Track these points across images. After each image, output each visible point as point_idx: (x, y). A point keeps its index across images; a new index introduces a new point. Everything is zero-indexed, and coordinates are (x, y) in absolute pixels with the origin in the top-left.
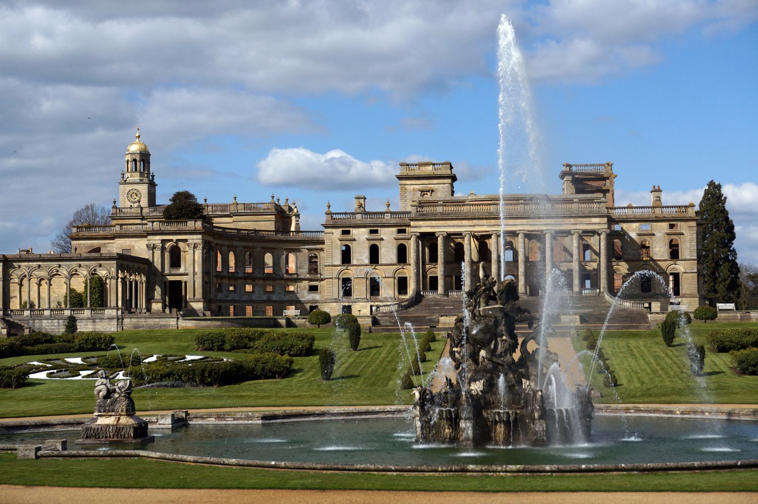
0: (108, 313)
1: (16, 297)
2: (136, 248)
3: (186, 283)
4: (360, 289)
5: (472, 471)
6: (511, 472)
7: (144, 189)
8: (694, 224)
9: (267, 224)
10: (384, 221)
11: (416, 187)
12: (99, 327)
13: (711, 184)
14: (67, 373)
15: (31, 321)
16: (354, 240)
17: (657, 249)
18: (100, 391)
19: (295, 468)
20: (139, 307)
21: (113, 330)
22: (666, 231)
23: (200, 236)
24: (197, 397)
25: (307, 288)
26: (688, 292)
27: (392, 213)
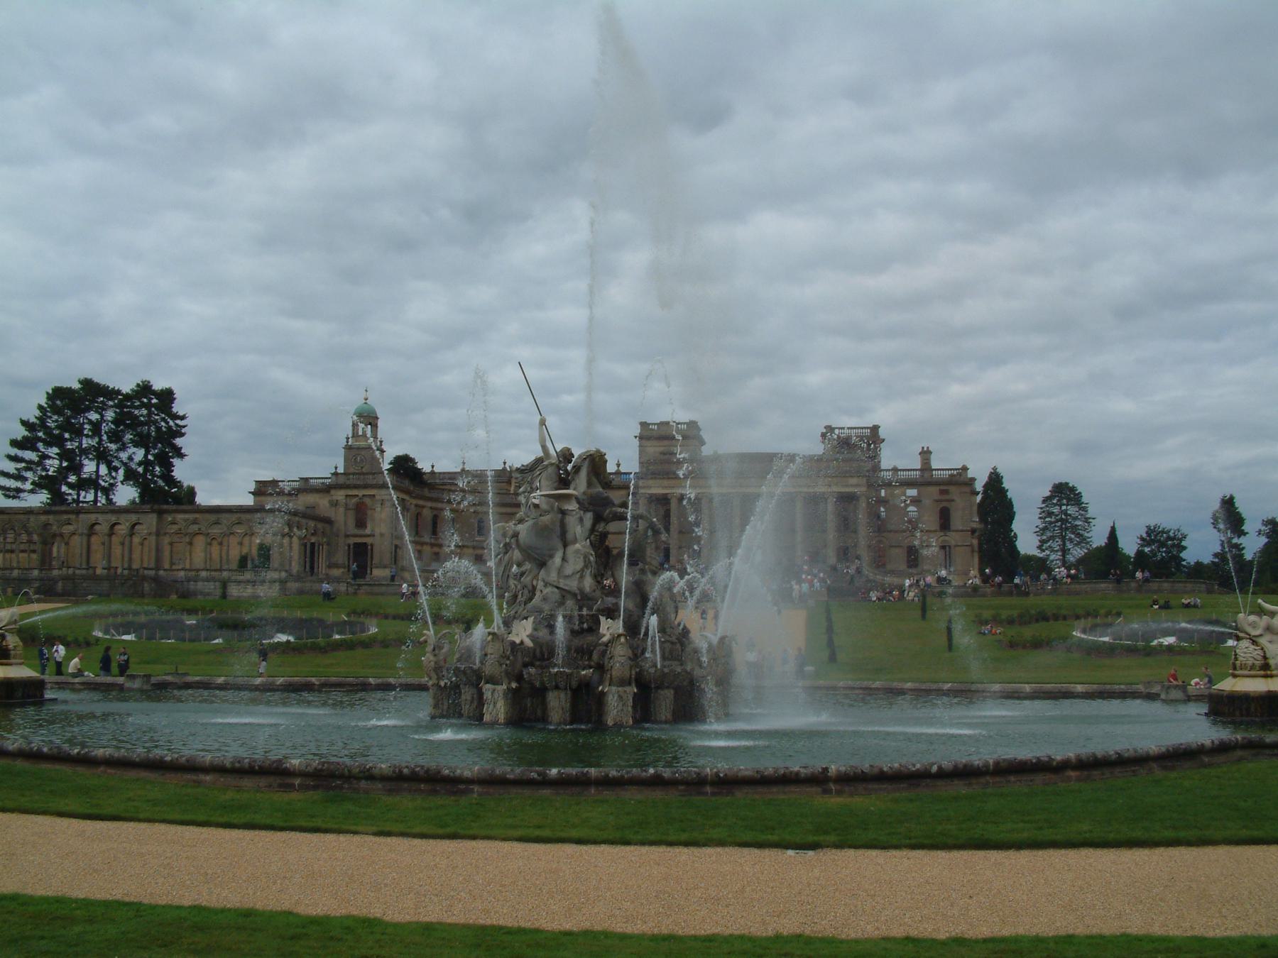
3: (372, 545)
15: (185, 583)
22: (936, 498)
24: (682, 650)
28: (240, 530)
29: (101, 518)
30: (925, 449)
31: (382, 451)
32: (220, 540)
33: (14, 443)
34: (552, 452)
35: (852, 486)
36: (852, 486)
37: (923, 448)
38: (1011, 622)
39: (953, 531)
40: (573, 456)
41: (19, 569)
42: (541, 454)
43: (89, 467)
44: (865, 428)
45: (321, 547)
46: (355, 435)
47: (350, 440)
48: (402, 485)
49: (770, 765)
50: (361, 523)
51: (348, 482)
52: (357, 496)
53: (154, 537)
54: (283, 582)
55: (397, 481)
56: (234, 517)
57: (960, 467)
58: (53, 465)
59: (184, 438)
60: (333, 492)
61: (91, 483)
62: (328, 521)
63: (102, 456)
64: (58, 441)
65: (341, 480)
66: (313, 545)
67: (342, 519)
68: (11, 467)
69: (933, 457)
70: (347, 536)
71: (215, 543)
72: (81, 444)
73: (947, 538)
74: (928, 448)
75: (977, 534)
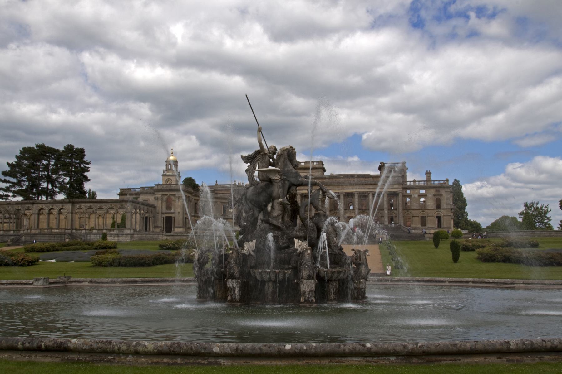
0: (127, 231)
1: (87, 225)
2: (150, 200)
3: (174, 217)
12: (121, 239)
13: (455, 180)
15: (86, 236)
17: (429, 203)
20: (148, 229)
21: (128, 240)
22: (433, 194)
28: (112, 211)
29: (44, 206)
30: (428, 172)
31: (180, 177)
32: (103, 216)
33: (4, 173)
34: (265, 147)
35: (395, 188)
36: (395, 188)
37: (427, 171)
39: (443, 209)
40: (276, 150)
41: (3, 230)
42: (259, 148)
43: (44, 185)
45: (150, 219)
46: (168, 170)
47: (165, 172)
48: (188, 190)
50: (169, 208)
51: (163, 189)
52: (167, 195)
53: (70, 215)
54: (132, 235)
55: (186, 188)
56: (109, 205)
57: (445, 179)
58: (25, 185)
59: (89, 172)
60: (156, 193)
61: (45, 192)
62: (154, 207)
63: (49, 180)
64: (27, 173)
65: (160, 188)
66: (146, 218)
67: (161, 206)
68: (4, 185)
69: (432, 175)
70: (162, 213)
71: (101, 217)
72: (39, 174)
73: (439, 212)
74: (429, 171)
75: (453, 211)
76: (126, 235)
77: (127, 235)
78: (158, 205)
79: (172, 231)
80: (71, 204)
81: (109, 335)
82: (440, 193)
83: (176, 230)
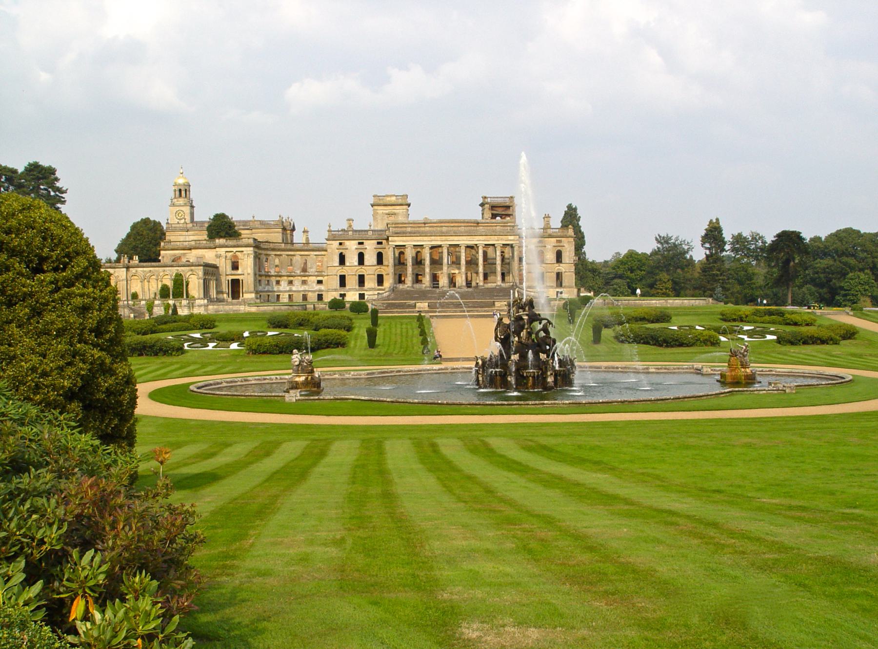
2: (206, 257)
3: (242, 280)
4: (352, 282)
5: (547, 404)
6: (566, 404)
7: (187, 210)
8: (572, 240)
9: (276, 236)
10: (367, 236)
11: (384, 211)
14: (199, 345)
16: (347, 249)
17: (548, 256)
18: (296, 361)
19: (469, 405)
23: (252, 249)
25: (316, 282)
26: (567, 284)
27: (372, 231)
38: (851, 470)
44: (506, 197)
49: (266, 358)
60: (217, 249)
70: (227, 275)
76: (198, 306)
77: (200, 306)
78: (221, 265)
79: (239, 297)
80: (125, 269)
81: (782, 376)
82: (561, 244)
83: (246, 296)
